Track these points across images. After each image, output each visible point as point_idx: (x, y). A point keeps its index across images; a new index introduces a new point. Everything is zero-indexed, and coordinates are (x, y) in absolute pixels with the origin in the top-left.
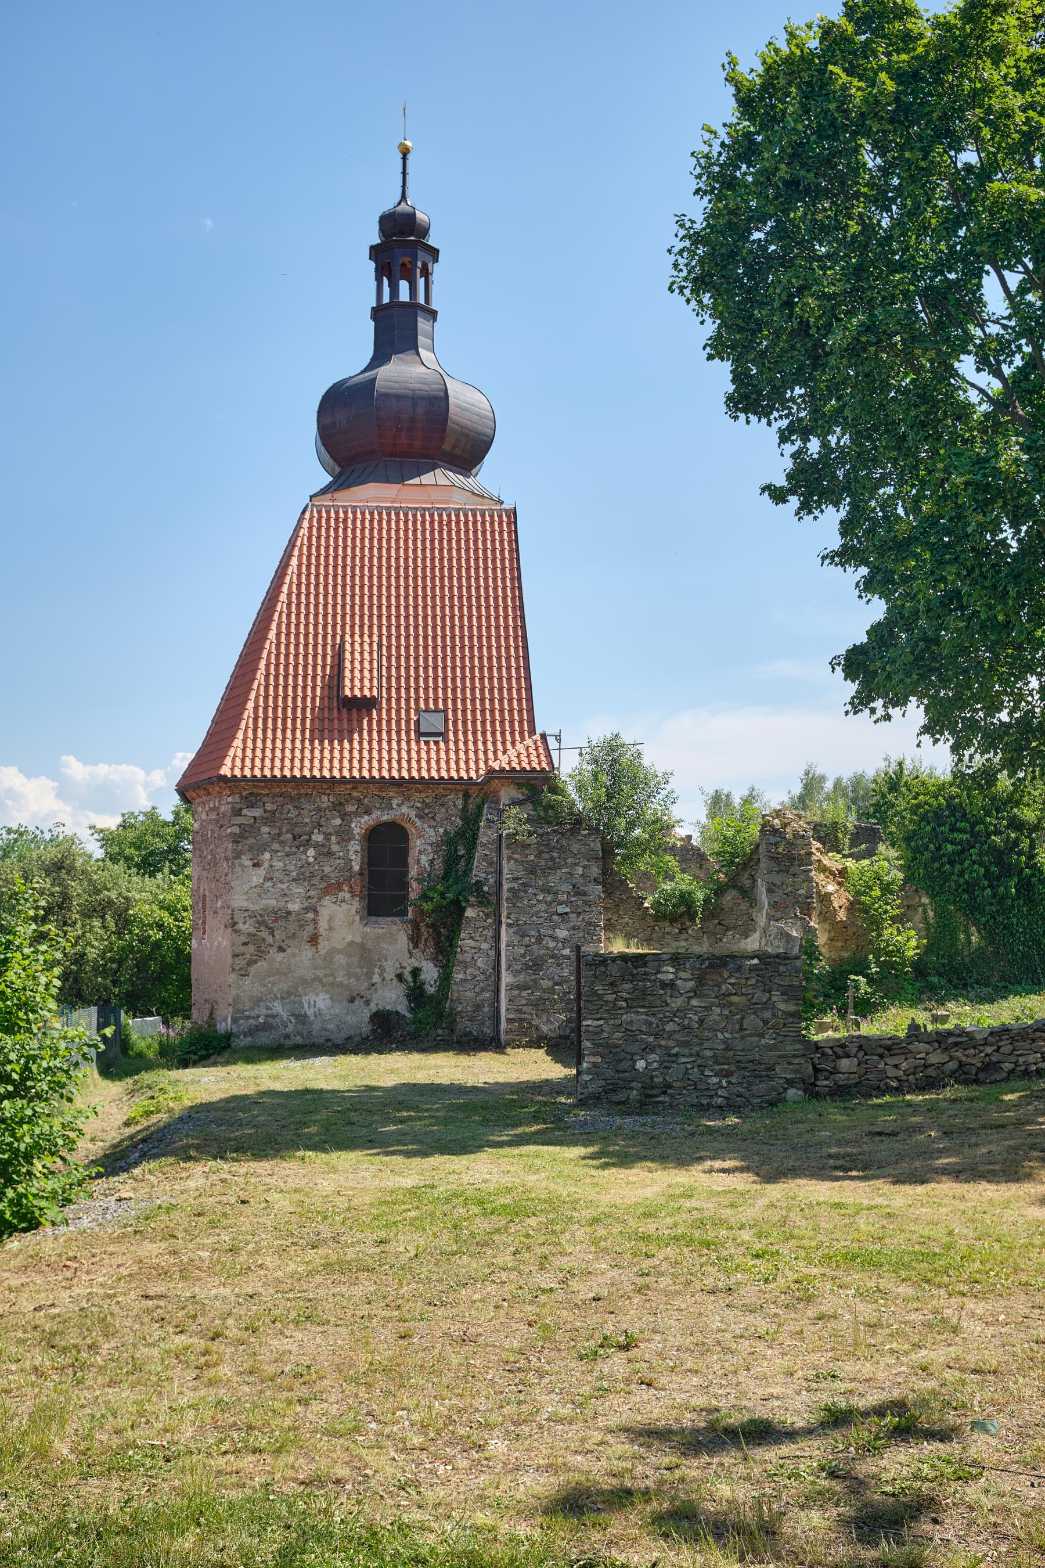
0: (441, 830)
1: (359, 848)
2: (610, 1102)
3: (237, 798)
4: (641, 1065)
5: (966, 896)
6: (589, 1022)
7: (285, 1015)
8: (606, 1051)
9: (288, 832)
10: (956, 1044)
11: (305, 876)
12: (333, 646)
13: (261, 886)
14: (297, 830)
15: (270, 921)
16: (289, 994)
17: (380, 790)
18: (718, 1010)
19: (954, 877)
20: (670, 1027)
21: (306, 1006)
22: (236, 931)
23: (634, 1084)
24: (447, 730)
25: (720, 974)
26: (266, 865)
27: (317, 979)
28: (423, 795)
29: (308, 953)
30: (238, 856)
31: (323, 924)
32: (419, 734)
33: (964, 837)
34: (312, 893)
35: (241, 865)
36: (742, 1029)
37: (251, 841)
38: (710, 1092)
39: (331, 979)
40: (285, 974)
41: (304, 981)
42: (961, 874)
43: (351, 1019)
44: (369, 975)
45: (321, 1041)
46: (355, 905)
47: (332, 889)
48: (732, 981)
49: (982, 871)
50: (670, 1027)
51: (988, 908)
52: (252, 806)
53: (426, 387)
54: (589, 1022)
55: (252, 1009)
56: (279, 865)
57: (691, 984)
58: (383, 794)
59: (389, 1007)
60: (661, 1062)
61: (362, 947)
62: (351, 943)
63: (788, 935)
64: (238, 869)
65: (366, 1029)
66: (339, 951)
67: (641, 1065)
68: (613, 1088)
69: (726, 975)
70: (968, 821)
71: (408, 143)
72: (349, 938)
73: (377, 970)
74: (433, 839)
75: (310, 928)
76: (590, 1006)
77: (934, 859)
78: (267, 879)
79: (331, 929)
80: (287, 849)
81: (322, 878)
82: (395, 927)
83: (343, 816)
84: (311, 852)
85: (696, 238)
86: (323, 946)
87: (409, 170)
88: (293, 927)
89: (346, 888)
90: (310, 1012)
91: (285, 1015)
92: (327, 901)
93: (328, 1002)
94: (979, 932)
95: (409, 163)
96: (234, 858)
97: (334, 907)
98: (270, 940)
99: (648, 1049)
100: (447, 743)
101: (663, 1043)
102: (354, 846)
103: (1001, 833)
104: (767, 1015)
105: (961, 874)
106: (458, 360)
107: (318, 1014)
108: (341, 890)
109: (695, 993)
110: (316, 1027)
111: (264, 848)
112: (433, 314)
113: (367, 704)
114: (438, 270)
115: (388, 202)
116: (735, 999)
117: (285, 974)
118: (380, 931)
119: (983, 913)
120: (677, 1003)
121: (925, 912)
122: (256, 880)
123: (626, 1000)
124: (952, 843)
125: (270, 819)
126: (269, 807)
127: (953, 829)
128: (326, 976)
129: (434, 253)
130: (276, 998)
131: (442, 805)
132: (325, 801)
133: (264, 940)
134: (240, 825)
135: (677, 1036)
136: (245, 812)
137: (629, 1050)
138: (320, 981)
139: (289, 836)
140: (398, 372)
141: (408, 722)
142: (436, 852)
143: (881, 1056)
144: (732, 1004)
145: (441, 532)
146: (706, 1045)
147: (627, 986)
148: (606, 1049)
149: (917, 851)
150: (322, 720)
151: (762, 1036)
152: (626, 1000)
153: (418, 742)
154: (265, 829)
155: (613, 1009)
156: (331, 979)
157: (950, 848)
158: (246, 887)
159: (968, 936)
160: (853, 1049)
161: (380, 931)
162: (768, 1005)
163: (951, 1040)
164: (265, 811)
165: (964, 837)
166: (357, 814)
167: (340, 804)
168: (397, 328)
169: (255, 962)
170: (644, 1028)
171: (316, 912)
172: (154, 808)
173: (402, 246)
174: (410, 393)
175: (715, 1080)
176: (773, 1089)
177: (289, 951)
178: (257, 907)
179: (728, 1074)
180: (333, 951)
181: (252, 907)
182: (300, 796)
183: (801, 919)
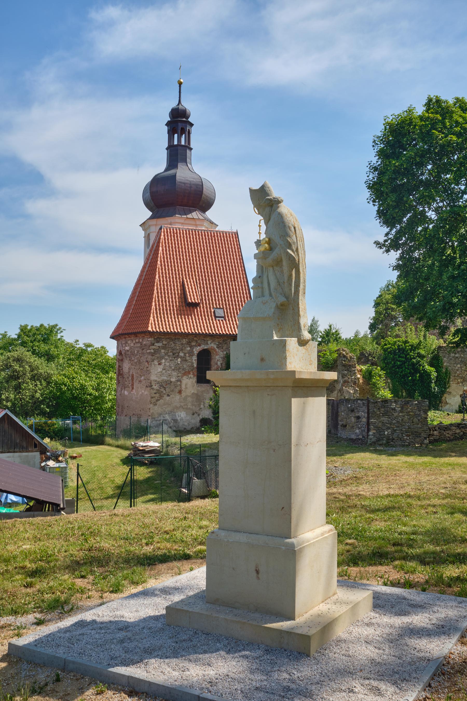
0: (225, 353)
1: (196, 359)
2: (378, 444)
3: (153, 339)
4: (386, 433)
5: (403, 380)
6: (372, 420)
7: (170, 420)
8: (377, 429)
9: (171, 352)
10: (462, 427)
11: (177, 368)
12: (180, 282)
13: (161, 372)
14: (174, 351)
15: (164, 385)
16: (171, 412)
17: (204, 337)
18: (407, 417)
19: (399, 373)
20: (394, 422)
21: (177, 416)
22: (153, 389)
23: (384, 439)
24: (225, 316)
25: (407, 406)
26: (163, 364)
27: (181, 407)
28: (219, 340)
29: (178, 397)
30: (153, 361)
31: (183, 386)
32: (216, 317)
33: (404, 359)
34: (179, 375)
35: (154, 364)
36: (413, 422)
37: (158, 355)
38: (404, 441)
39: (186, 406)
40: (170, 405)
41: (177, 408)
42: (402, 372)
43: (193, 421)
44: (199, 405)
45: (183, 429)
46: (195, 379)
47: (186, 373)
48: (410, 408)
49: (409, 371)
50: (394, 422)
51: (409, 384)
52: (158, 342)
53: (195, 180)
54: (372, 420)
55: (158, 417)
56: (168, 364)
57: (400, 409)
58: (205, 339)
59: (206, 417)
60: (392, 432)
61: (197, 394)
62: (193, 394)
63: (350, 392)
64: (153, 365)
65: (198, 424)
66: (189, 396)
67: (386, 433)
68: (379, 440)
69: (409, 406)
70: (404, 354)
71: (182, 80)
72: (193, 391)
73: (202, 403)
74: (222, 356)
75: (179, 388)
76: (373, 415)
77: (393, 367)
78: (163, 369)
79: (186, 388)
80: (171, 358)
81: (183, 369)
82: (208, 388)
83: (191, 347)
84: (179, 360)
85: (375, 169)
86: (183, 394)
87: (182, 91)
88: (173, 387)
89: (192, 373)
90: (179, 419)
91: (170, 420)
92: (185, 378)
93: (185, 415)
94: (406, 392)
95: (182, 88)
96: (152, 361)
97: (187, 380)
98: (164, 392)
99: (388, 428)
100: (226, 320)
101: (392, 426)
102: (195, 358)
103: (415, 359)
104: (419, 418)
105: (402, 372)
106: (201, 167)
107: (182, 419)
108: (190, 374)
109: (401, 411)
110: (181, 424)
111: (162, 358)
112: (191, 149)
113: (196, 305)
114: (193, 129)
115: (173, 104)
116: (411, 413)
117: (170, 405)
118: (204, 389)
119: (408, 385)
120: (396, 414)
121: (389, 385)
122: (160, 370)
123: (382, 414)
124: (399, 361)
125: (164, 347)
126: (164, 343)
127: (399, 357)
128: (184, 405)
129: (192, 125)
130: (167, 413)
131: (225, 343)
132: (184, 341)
133: (162, 392)
134: (154, 349)
135: (396, 424)
136: (156, 344)
137: (383, 428)
138: (182, 407)
139: (171, 354)
140: (181, 173)
141: (211, 312)
142: (223, 361)
143: (444, 431)
144: (410, 415)
145: (212, 239)
146: (403, 427)
147: (383, 409)
148: (377, 428)
149: (387, 363)
150: (180, 310)
151: (418, 424)
152: (382, 414)
153: (216, 320)
154: (163, 351)
155: (379, 417)
156: (186, 406)
157: (399, 363)
158: (156, 372)
159: (402, 393)
160: (437, 428)
161: (204, 389)
162: (419, 415)
163: (461, 426)
164: (163, 344)
165: (404, 359)
166: (195, 346)
167: (190, 342)
168: (177, 154)
169: (159, 400)
170: (387, 422)
171: (181, 382)
172: (5, 332)
173: (179, 122)
174: (189, 182)
175: (406, 437)
176: (421, 440)
177: (171, 396)
178: (160, 380)
179: (409, 436)
180: (187, 396)
181: (158, 380)
182: (175, 339)
183: (353, 387)
